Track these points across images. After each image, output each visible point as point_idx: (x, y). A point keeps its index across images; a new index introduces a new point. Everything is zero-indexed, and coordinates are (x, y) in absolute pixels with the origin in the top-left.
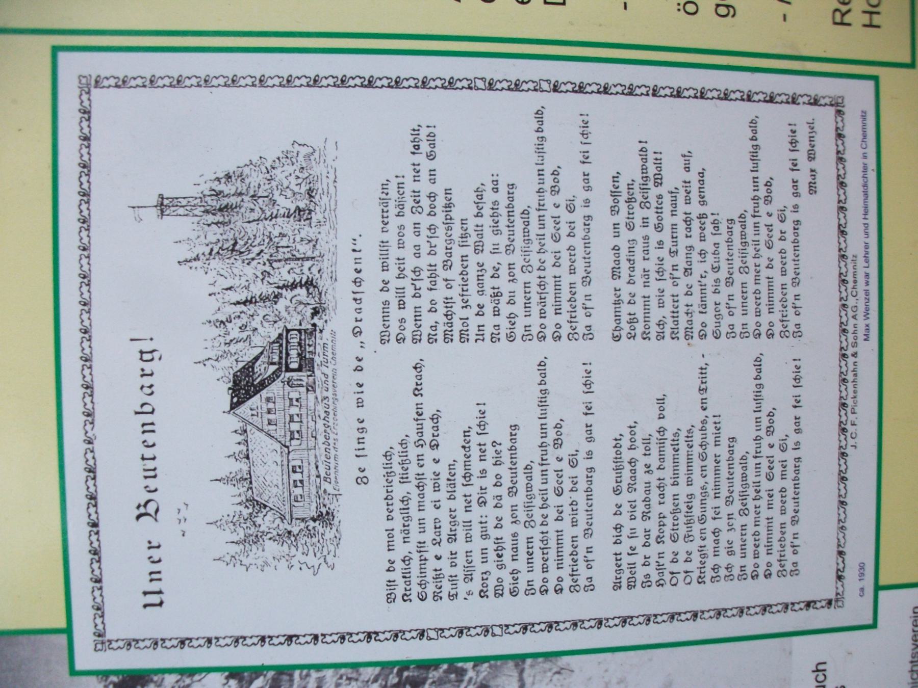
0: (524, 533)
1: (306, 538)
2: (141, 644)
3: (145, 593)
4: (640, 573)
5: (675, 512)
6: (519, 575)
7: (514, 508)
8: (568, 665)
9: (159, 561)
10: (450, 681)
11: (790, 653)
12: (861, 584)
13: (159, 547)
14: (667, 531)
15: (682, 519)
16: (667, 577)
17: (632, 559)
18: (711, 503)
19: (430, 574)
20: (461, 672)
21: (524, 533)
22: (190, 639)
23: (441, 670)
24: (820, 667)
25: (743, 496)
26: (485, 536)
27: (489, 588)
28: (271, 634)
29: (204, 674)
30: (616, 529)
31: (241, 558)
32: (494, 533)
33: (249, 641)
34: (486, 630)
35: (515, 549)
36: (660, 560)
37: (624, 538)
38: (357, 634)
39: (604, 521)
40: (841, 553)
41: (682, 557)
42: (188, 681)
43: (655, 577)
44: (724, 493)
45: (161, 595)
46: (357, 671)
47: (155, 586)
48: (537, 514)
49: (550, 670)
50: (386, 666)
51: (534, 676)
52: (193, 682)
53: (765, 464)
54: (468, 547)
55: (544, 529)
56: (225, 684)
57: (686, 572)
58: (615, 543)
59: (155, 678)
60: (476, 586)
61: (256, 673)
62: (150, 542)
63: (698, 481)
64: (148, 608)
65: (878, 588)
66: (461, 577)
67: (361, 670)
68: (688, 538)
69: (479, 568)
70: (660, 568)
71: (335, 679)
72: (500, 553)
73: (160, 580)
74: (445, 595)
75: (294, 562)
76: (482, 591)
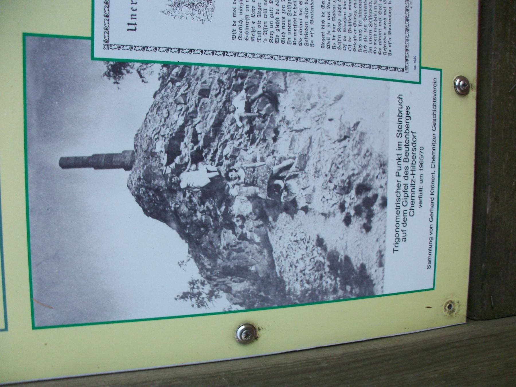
0: (287, 18)
1: (200, 7)
2: (125, 48)
3: (128, 24)
4: (332, 42)
5: (345, 19)
6: (285, 35)
7: (283, 7)
8: (304, 77)
9: (136, 10)
10: (256, 78)
11: (389, 88)
12: (415, 65)
13: (136, 3)
14: (342, 26)
15: (347, 24)
16: (342, 46)
17: (329, 36)
18: (358, 19)
19: (250, 30)
20: (261, 74)
21: (287, 18)
22: (147, 47)
23: (253, 72)
24: (400, 97)
25: (370, 19)
26: (272, 16)
27: (273, 39)
28: (183, 48)
29: (152, 64)
30: (322, 22)
31: (172, 12)
32: (276, 16)
33: (173, 50)
34: (272, 57)
35: (284, 24)
36: (339, 38)
37: (325, 27)
38: (219, 52)
39: (318, 19)
40: (407, 50)
41: (347, 39)
42: (145, 66)
43: (337, 45)
44: (363, 16)
45: (136, 26)
46: (219, 69)
47: (133, 21)
48: (292, 11)
49: (297, 78)
50: (231, 68)
51: (290, 80)
52: (147, 67)
53: (378, 8)
54: (266, 20)
55: (295, 17)
56: (161, 69)
57: (349, 45)
58: (322, 28)
59: (130, 64)
60: (268, 37)
61: (175, 65)
62: (132, 1)
63: (353, 9)
64: (129, 31)
65: (421, 68)
66: (262, 32)
67: (220, 68)
68: (349, 31)
69: (270, 30)
70: (339, 42)
71: (209, 71)
72: (278, 24)
73: (136, 18)
74: (255, 39)
75: (195, 17)
76: (270, 39)
